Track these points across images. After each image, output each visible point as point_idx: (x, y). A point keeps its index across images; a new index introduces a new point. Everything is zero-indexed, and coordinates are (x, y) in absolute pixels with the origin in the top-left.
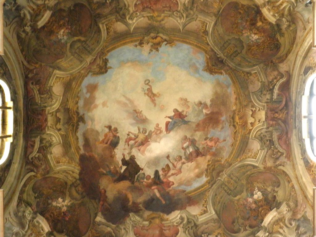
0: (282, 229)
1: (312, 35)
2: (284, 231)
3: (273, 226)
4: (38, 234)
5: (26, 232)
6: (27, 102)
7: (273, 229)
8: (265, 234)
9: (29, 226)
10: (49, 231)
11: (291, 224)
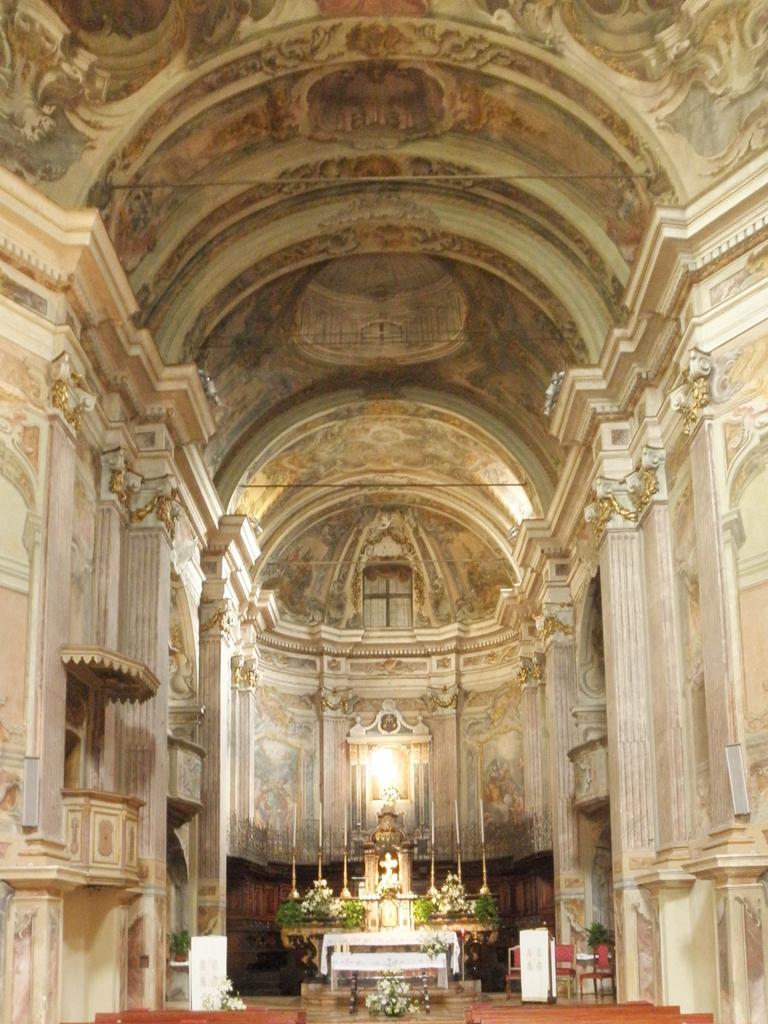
0: (729, 43)
1: (454, 488)
2: (729, 53)
3: (710, 23)
4: (41, 58)
5: (12, 66)
6: (187, 526)
7: (706, 31)
8: (681, 40)
9: (11, 45)
10: (65, 35)
11: (755, 39)
